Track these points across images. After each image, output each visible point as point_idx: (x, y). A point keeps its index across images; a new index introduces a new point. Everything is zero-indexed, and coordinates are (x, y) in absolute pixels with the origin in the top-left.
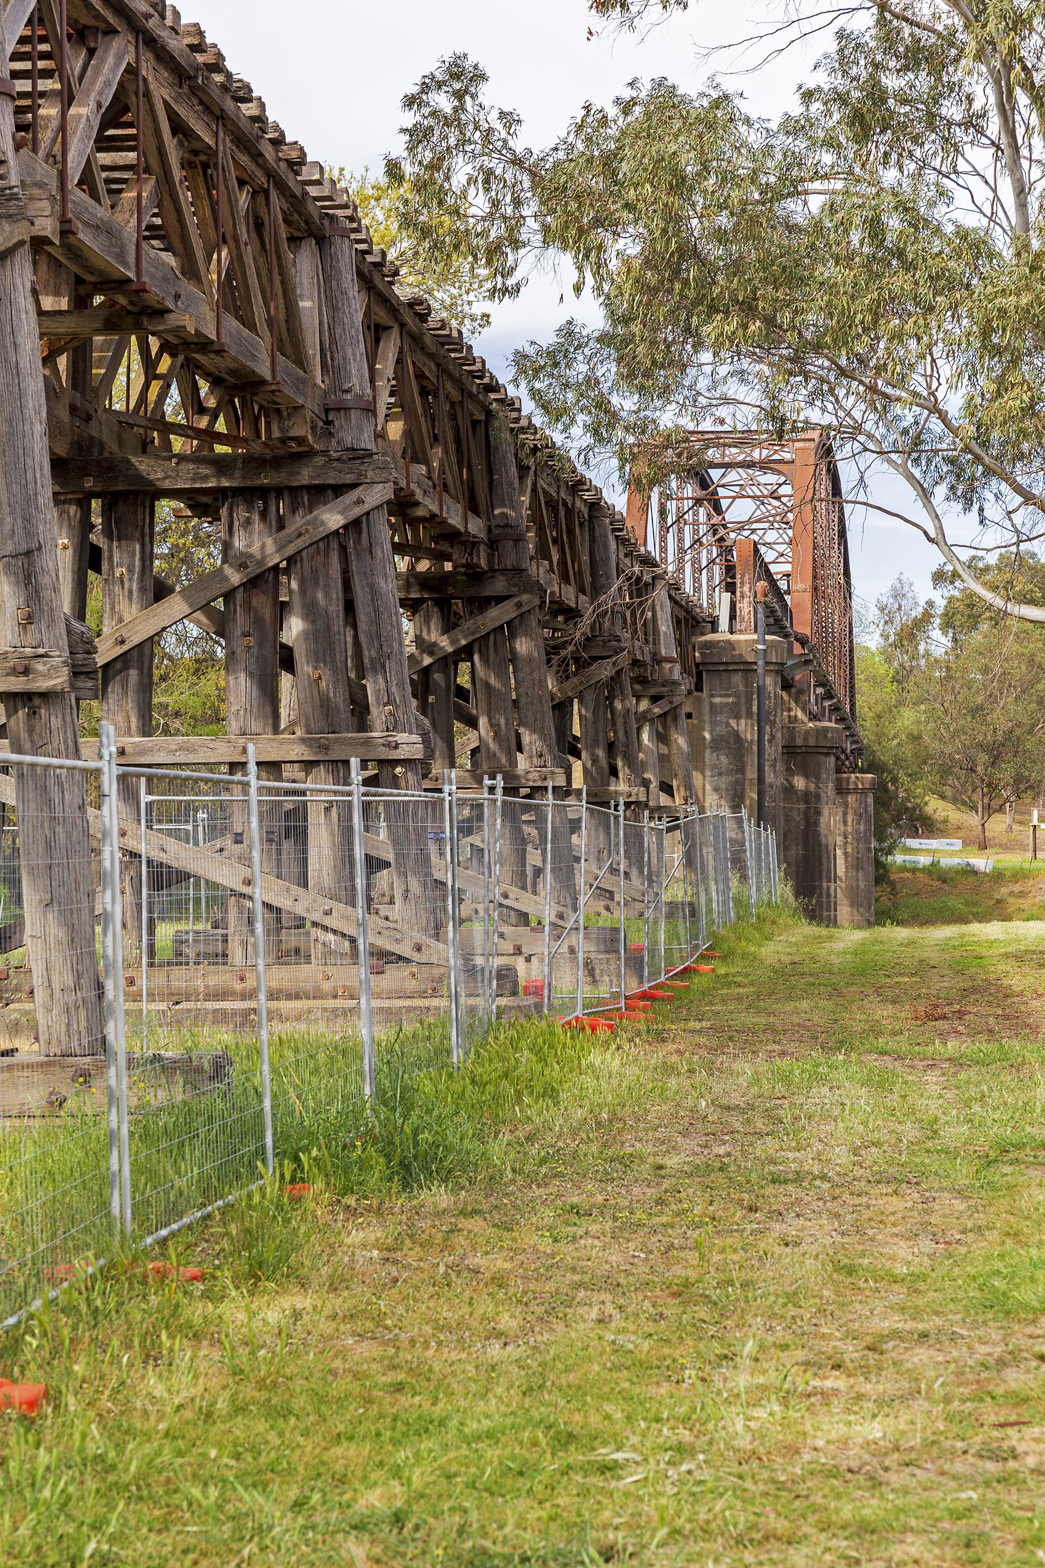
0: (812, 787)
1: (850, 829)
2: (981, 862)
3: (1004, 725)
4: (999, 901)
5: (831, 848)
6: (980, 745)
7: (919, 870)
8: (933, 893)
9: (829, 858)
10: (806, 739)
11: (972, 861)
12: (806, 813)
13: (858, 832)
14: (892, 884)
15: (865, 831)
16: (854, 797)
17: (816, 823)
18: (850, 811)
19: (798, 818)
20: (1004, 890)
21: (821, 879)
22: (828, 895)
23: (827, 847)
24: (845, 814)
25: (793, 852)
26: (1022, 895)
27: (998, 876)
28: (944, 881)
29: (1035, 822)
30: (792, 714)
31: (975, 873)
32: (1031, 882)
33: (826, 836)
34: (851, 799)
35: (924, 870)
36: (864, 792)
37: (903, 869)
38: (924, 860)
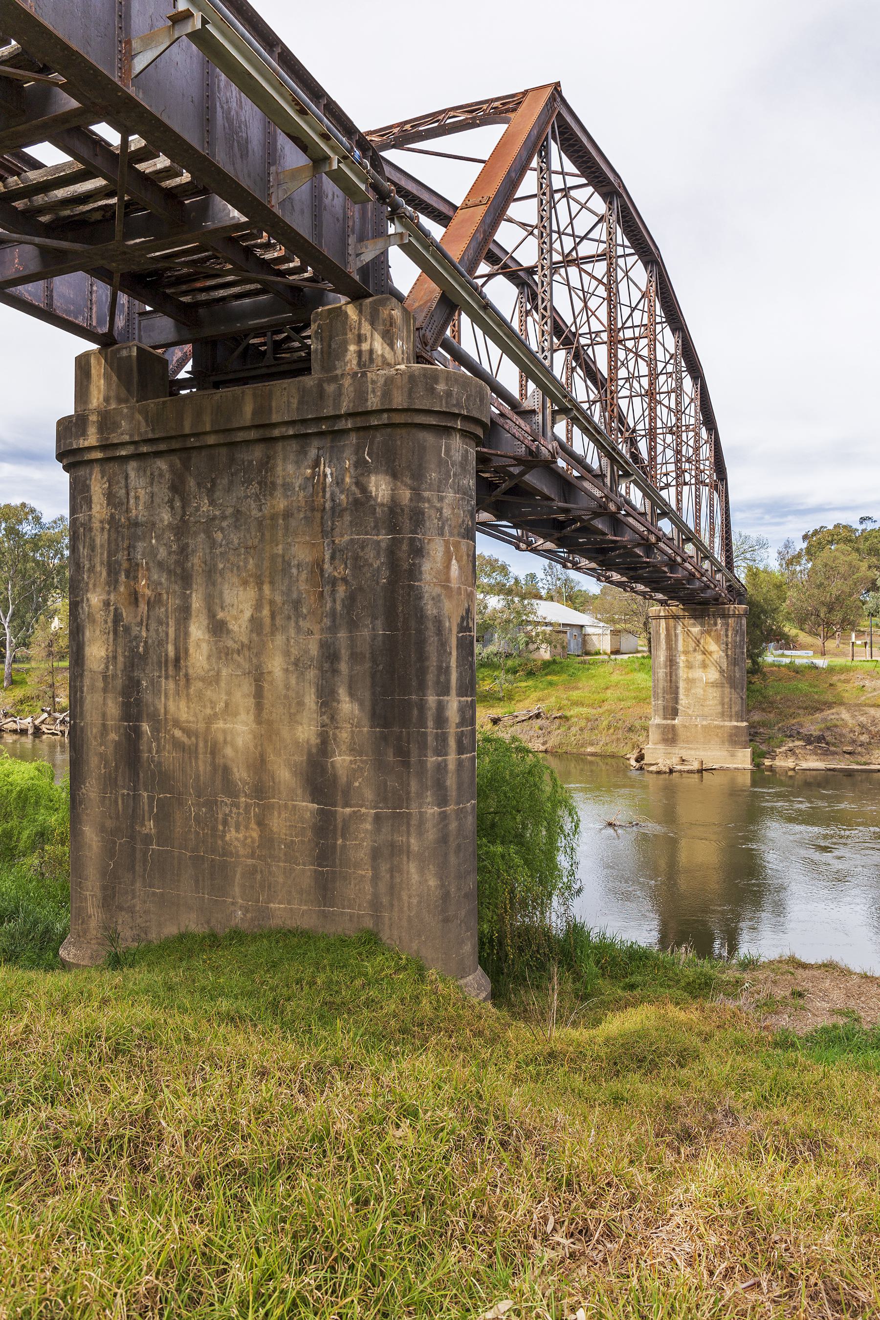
0: (406, 495)
1: (730, 640)
2: (821, 662)
3: (835, 592)
4: (831, 685)
5: (452, 625)
6: (823, 603)
7: (783, 666)
8: (790, 679)
9: (443, 645)
10: (387, 394)
11: (815, 661)
12: (392, 552)
13: (735, 642)
14: (764, 674)
15: (740, 641)
16: (733, 619)
17: (414, 573)
18: (730, 629)
19: (377, 561)
20: (835, 678)
21: (422, 687)
22: (441, 720)
23: (438, 622)
24: (727, 630)
25: (366, 633)
26: (847, 681)
27: (831, 670)
28: (797, 673)
29: (853, 640)
30: (365, 346)
31: (817, 668)
32: (852, 674)
33: (437, 599)
34: (731, 621)
35: (785, 666)
36: (739, 616)
37: (773, 665)
38: (787, 661)
